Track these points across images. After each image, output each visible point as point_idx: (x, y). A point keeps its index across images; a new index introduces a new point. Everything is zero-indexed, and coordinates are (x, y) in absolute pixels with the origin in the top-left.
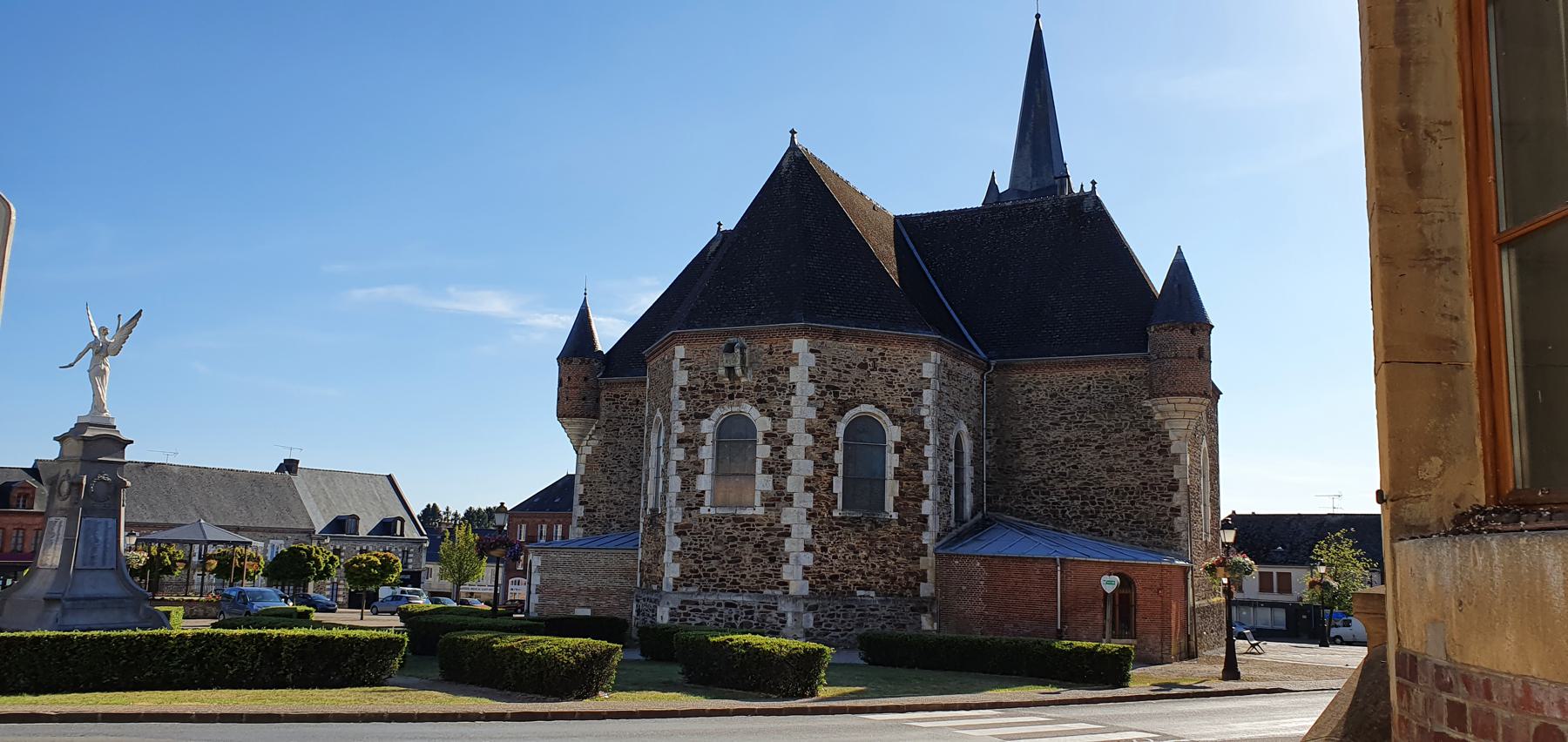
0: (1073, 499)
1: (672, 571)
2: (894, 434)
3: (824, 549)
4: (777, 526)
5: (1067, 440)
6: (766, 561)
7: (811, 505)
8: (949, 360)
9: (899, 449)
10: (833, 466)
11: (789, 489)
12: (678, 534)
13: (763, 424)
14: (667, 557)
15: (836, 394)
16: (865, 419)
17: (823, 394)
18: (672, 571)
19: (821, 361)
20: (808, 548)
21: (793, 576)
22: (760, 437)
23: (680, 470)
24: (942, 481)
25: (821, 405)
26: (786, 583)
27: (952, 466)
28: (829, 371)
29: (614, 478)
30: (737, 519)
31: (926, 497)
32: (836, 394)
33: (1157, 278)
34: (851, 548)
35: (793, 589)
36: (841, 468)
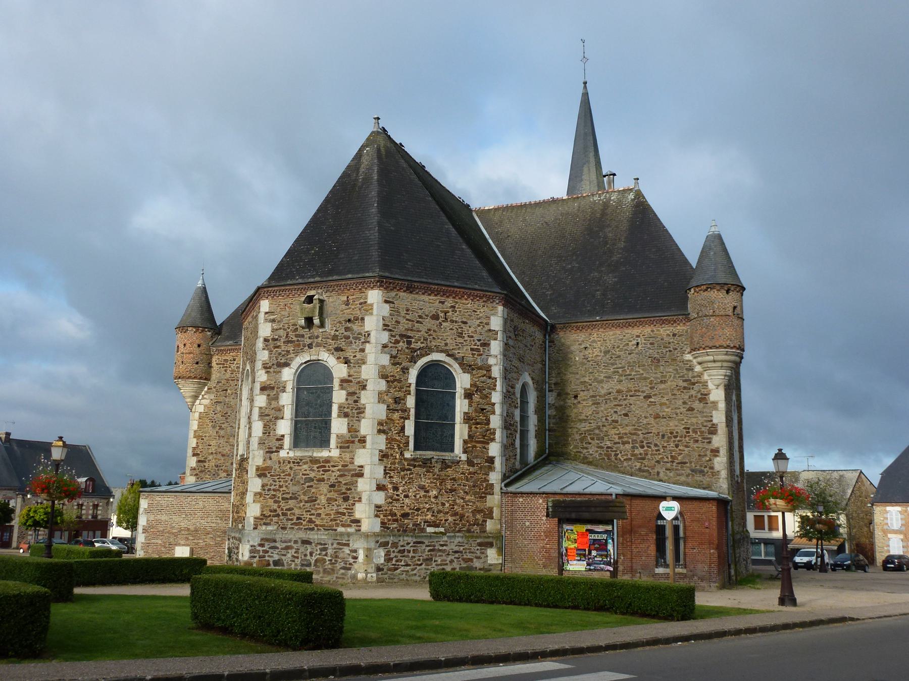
0: (624, 443)
1: (253, 510)
2: (463, 381)
3: (396, 489)
4: (350, 467)
5: (619, 392)
6: (340, 501)
7: (383, 447)
8: (515, 316)
9: (468, 395)
10: (406, 410)
11: (363, 432)
12: (259, 476)
13: (339, 371)
14: (249, 498)
15: (409, 343)
16: (434, 365)
17: (397, 342)
18: (253, 510)
19: (395, 311)
20: (380, 488)
21: (363, 511)
22: (336, 384)
23: (262, 415)
24: (508, 425)
25: (394, 353)
26: (358, 521)
27: (517, 413)
28: (402, 321)
29: (222, 433)
30: (314, 461)
31: (493, 440)
32: (409, 343)
33: (692, 252)
34: (422, 487)
35: (365, 527)
36: (412, 412)
